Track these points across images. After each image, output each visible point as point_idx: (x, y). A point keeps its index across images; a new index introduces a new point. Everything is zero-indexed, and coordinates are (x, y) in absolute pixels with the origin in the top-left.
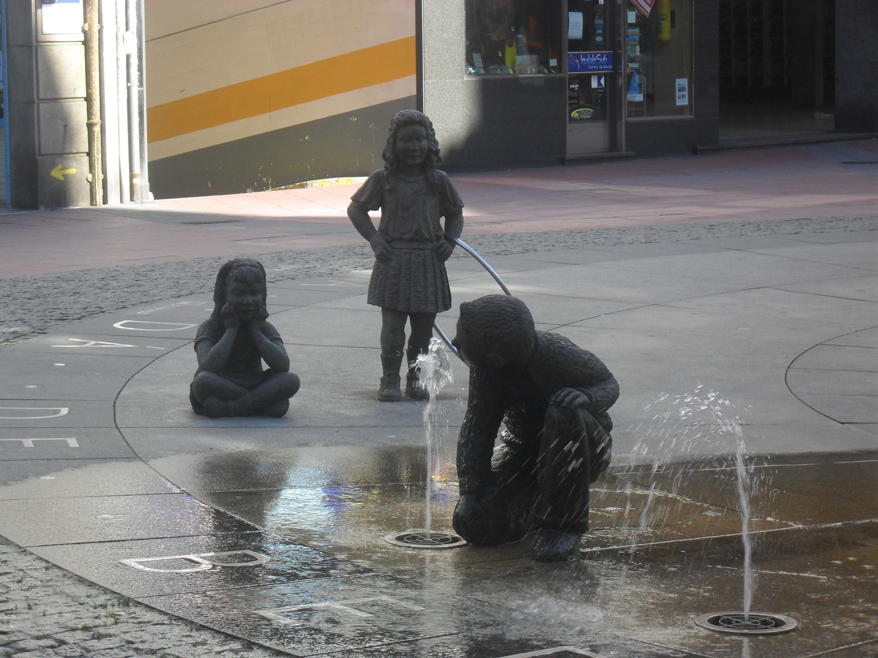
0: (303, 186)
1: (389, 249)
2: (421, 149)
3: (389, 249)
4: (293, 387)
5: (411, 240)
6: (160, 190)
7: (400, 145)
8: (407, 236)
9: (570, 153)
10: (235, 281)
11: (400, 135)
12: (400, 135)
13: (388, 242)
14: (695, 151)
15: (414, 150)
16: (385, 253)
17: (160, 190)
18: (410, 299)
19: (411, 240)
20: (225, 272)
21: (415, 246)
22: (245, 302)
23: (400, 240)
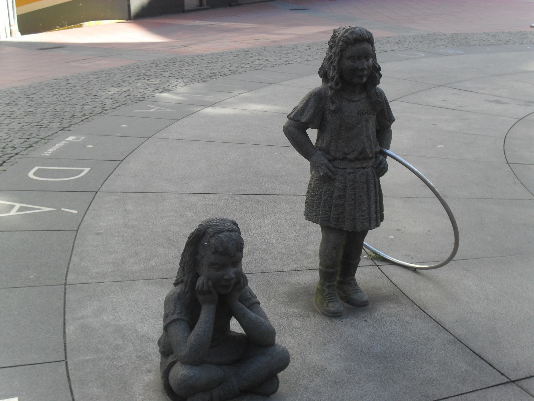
0: (81, 26)
1: (333, 169)
2: (369, 67)
3: (333, 169)
4: (284, 361)
5: (357, 159)
6: (24, 29)
7: (348, 63)
8: (351, 156)
9: (186, 8)
10: (214, 253)
11: (348, 53)
12: (348, 53)
13: (330, 161)
14: (230, 5)
15: (363, 70)
16: (330, 174)
17: (24, 29)
18: (355, 218)
19: (357, 159)
20: (197, 241)
21: (358, 165)
22: (226, 277)
23: (344, 159)
